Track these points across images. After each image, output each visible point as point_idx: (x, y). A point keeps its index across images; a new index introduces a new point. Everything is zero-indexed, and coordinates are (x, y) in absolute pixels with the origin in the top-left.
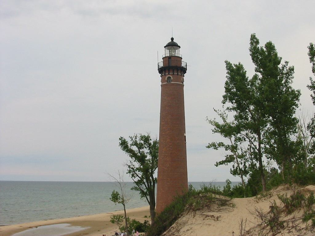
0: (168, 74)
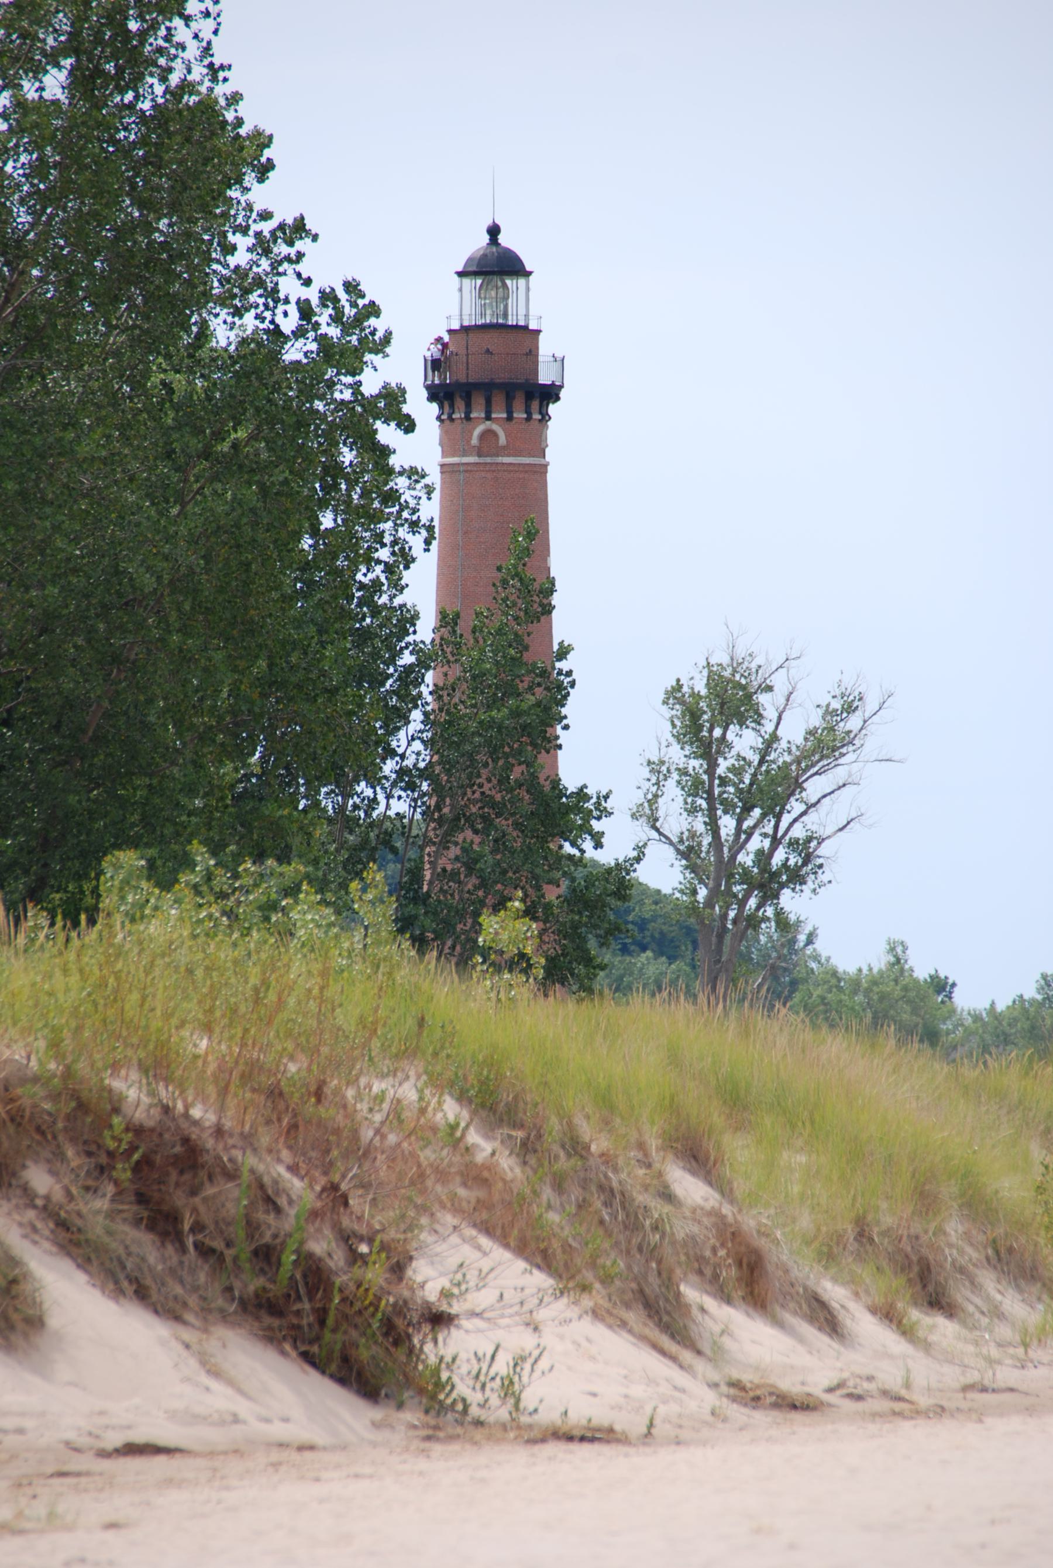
0: (483, 415)
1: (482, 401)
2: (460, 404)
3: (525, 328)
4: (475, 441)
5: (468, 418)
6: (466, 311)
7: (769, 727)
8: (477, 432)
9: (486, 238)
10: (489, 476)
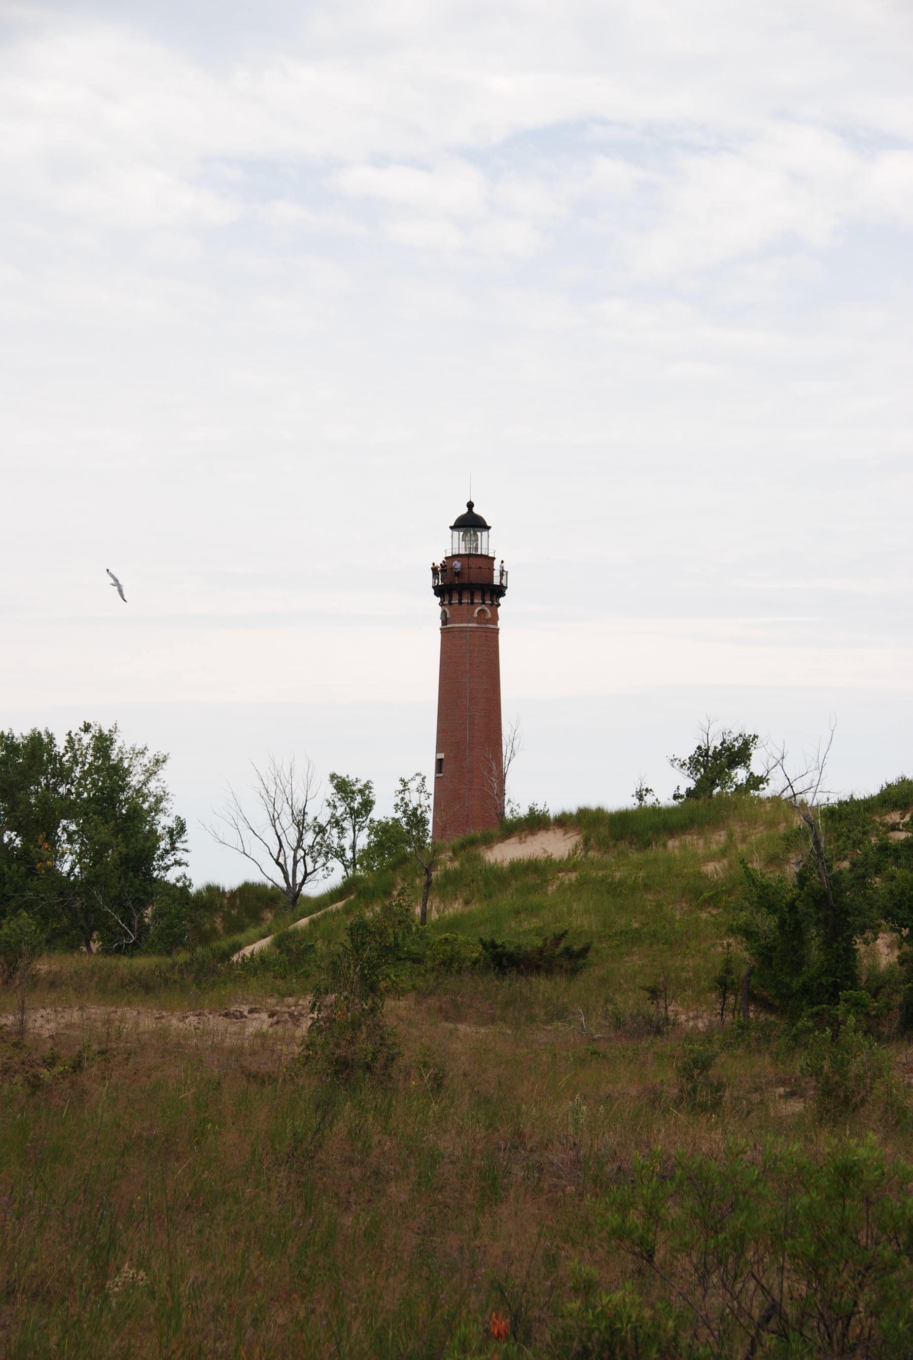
1: (457, 597)
2: (447, 597)
3: (487, 556)
4: (476, 615)
6: (456, 545)
7: (249, 1016)
8: (477, 611)
9: (465, 510)
10: (484, 634)
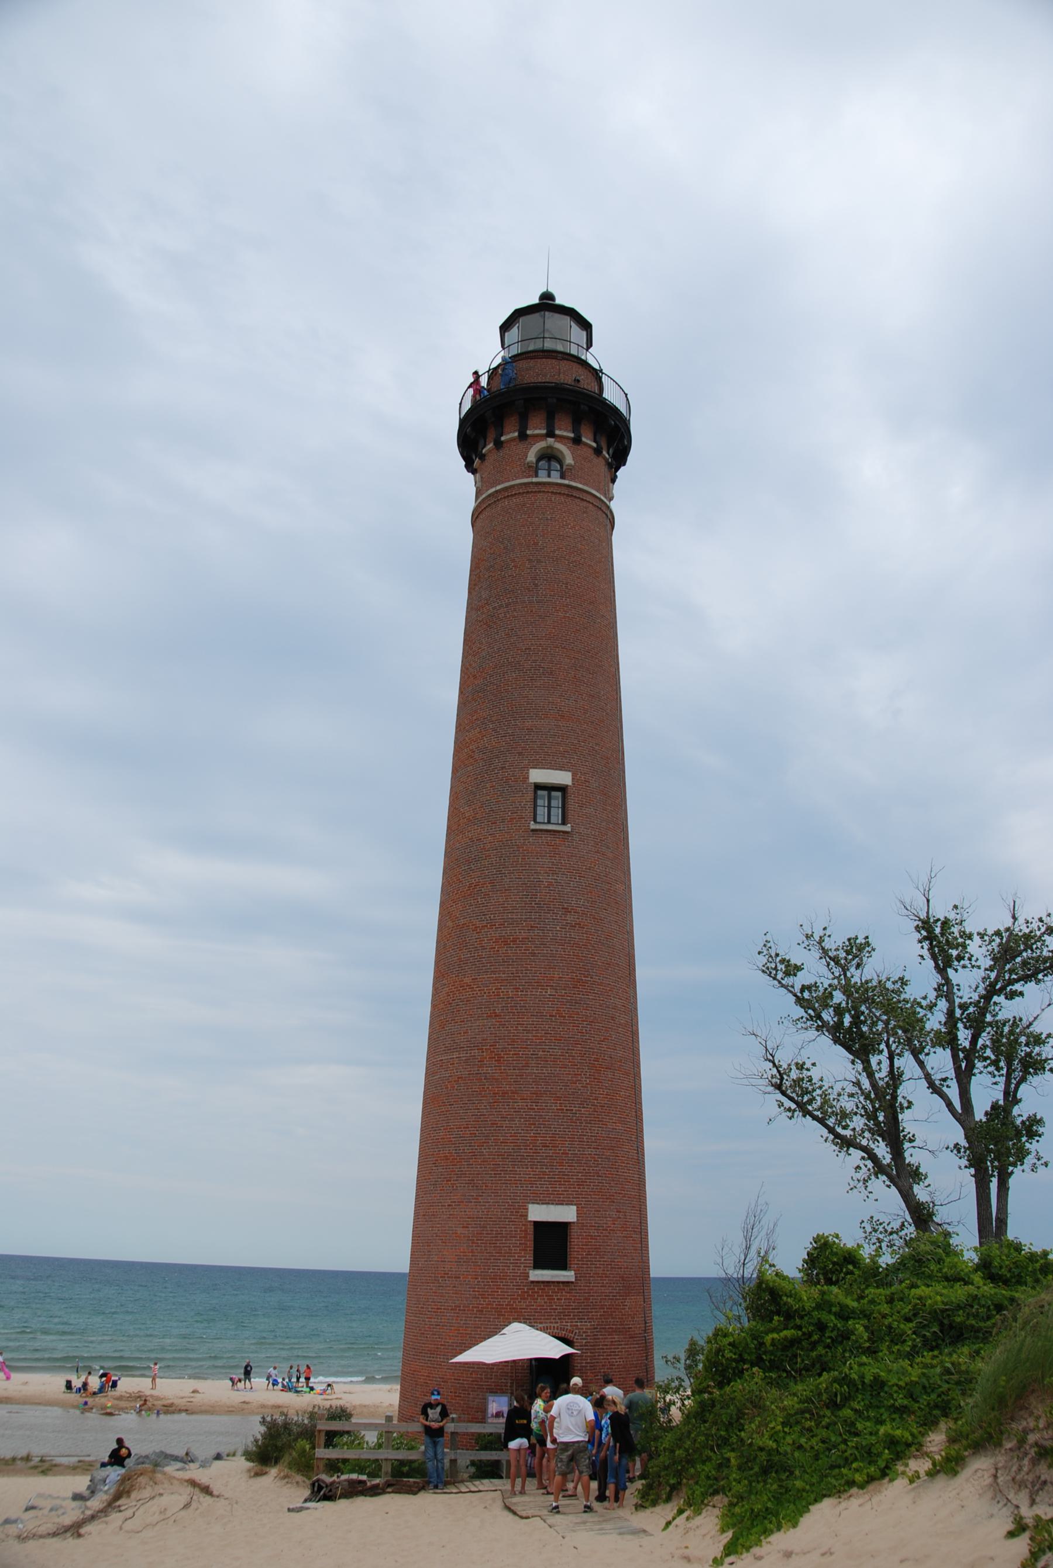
5: (523, 436)
